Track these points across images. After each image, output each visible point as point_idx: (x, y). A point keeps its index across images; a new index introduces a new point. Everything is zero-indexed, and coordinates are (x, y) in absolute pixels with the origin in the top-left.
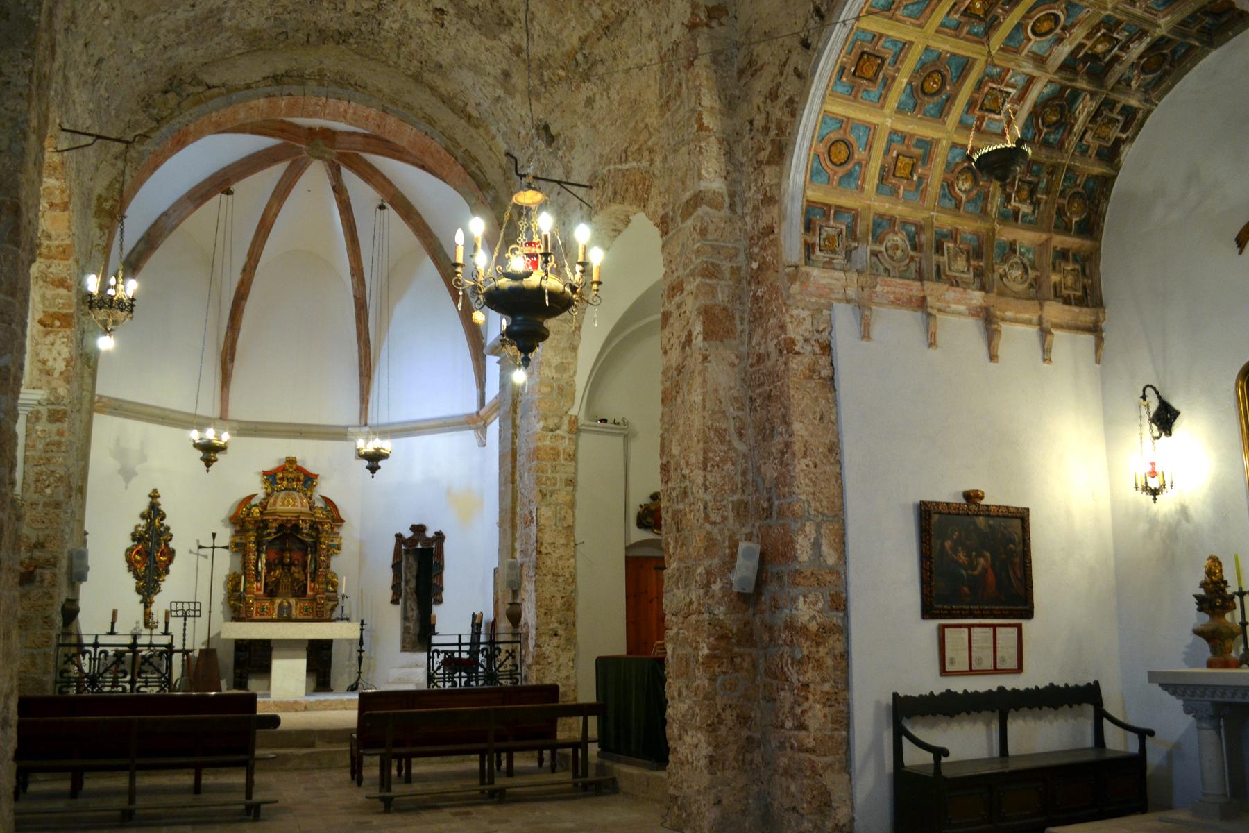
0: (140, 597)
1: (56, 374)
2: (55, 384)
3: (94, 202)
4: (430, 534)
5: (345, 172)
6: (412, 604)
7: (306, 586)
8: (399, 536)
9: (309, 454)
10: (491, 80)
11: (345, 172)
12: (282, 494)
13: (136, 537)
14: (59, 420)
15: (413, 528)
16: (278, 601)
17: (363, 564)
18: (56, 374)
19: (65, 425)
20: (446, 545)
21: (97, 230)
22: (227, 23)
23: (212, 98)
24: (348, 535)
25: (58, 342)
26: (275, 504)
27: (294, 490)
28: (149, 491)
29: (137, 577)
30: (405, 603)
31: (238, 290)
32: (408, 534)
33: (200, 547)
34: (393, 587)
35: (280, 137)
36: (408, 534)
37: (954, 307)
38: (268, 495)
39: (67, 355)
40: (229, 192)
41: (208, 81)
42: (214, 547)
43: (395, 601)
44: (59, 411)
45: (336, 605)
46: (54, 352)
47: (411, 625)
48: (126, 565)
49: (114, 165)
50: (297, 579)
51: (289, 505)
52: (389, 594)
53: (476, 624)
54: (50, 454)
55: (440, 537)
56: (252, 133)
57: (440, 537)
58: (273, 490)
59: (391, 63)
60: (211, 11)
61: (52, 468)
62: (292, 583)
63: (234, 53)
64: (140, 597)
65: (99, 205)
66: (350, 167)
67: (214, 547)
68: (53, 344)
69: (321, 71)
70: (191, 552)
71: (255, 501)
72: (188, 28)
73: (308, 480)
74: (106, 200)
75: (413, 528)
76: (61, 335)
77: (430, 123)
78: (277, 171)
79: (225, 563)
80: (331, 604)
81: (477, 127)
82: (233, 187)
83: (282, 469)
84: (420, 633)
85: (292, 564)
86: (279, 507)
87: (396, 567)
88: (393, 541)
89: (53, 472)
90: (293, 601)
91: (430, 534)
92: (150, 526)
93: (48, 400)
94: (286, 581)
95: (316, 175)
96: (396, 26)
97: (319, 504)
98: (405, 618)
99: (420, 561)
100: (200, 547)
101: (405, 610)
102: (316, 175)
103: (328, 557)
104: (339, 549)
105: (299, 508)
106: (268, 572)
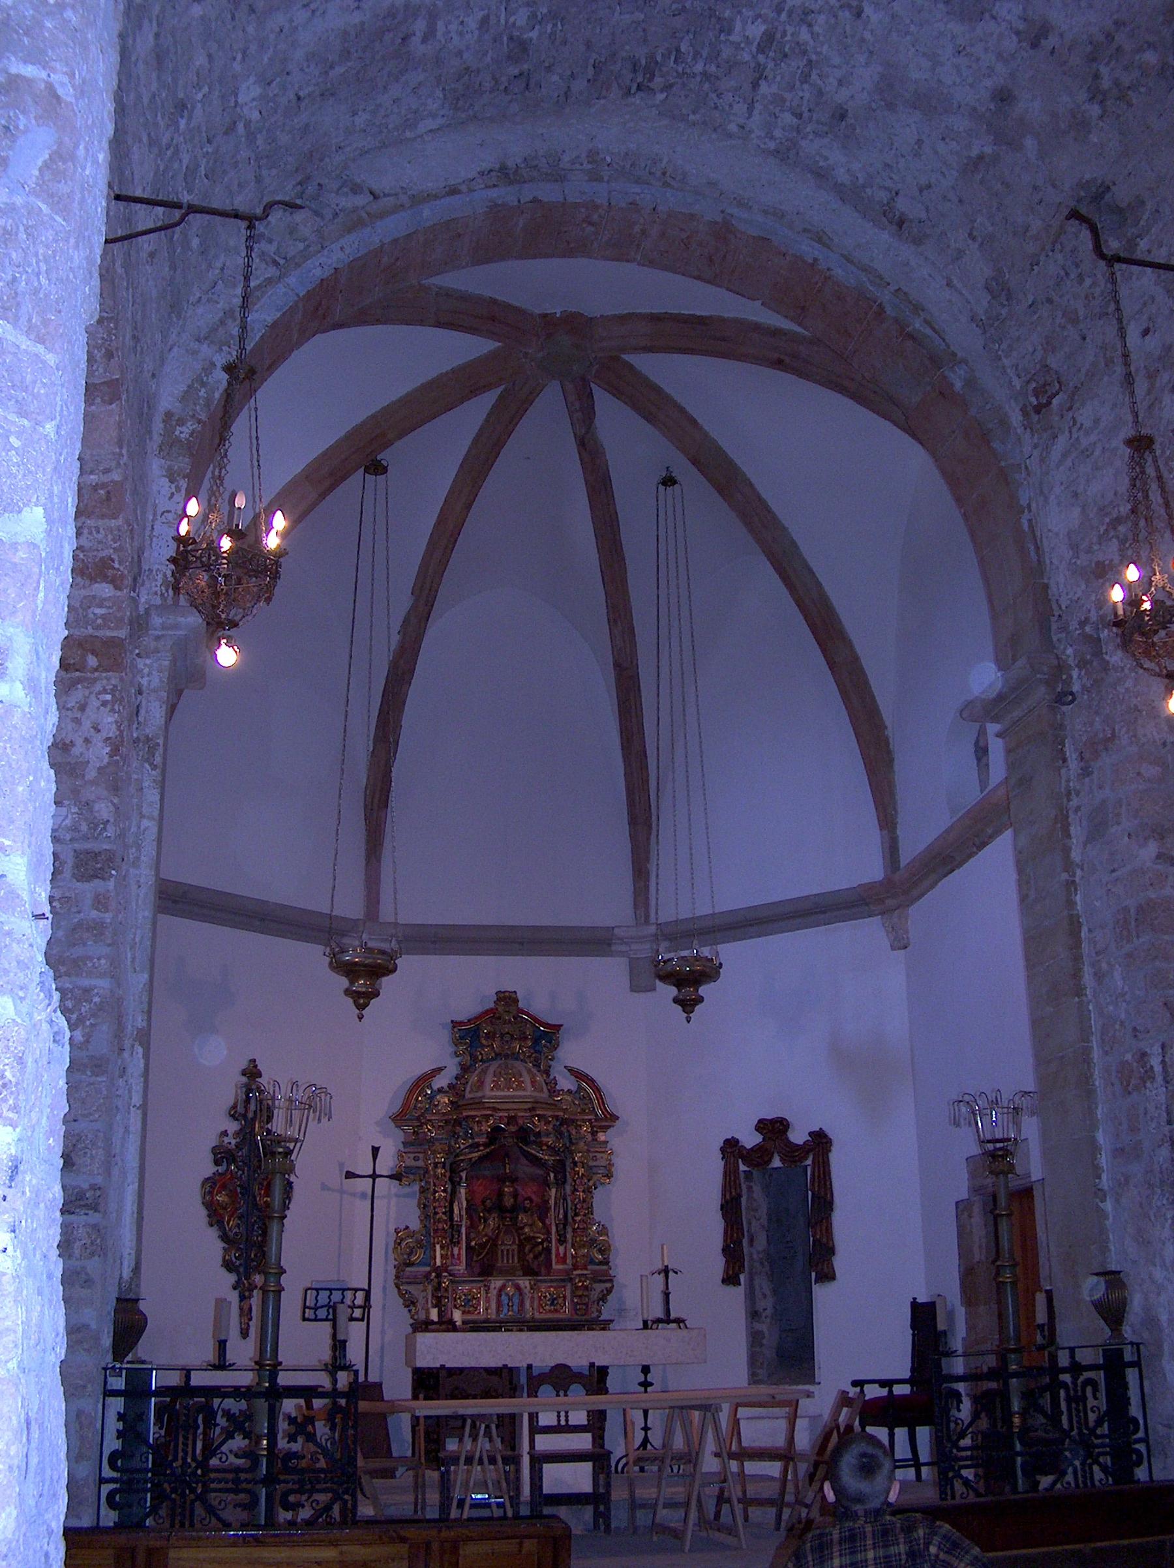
0: (232, 1278)
1: (91, 774)
2: (89, 793)
3: (158, 426)
4: (798, 1136)
5: (604, 402)
6: (763, 1284)
7: (548, 1250)
8: (731, 1148)
9: (541, 985)
10: (961, 123)
11: (604, 402)
12: (494, 1066)
13: (221, 1155)
14: (98, 875)
15: (763, 1126)
16: (496, 1283)
17: (657, 1205)
18: (91, 774)
19: (111, 884)
20: (836, 1158)
21: (165, 481)
22: (417, 47)
23: (382, 215)
24: (626, 1147)
25: (94, 703)
26: (481, 1083)
27: (515, 1056)
28: (244, 1064)
29: (224, 1237)
30: (751, 1280)
31: (394, 666)
32: (751, 1140)
33: (350, 1175)
34: (726, 1250)
35: (492, 335)
36: (751, 1140)
37: (282, 1477)
38: (465, 1069)
39: (113, 732)
40: (377, 468)
41: (375, 187)
42: (374, 1176)
43: (730, 1279)
44: (97, 854)
45: (609, 1291)
46: (87, 724)
47: (763, 1327)
48: (203, 1212)
49: (195, 353)
50: (530, 1239)
51: (505, 1091)
52: (718, 1264)
53: (923, 1316)
54: (78, 951)
55: (820, 1141)
56: (438, 325)
57: (820, 1141)
58: (474, 1058)
59: (733, 127)
60: (391, 13)
61: (86, 982)
62: (521, 1246)
63: (422, 128)
64: (232, 1278)
65: (168, 432)
66: (616, 392)
67: (374, 1176)
68: (83, 708)
69: (592, 155)
70: (324, 1187)
71: (441, 1082)
72: (346, 54)
73: (543, 1038)
74: (181, 422)
75: (763, 1126)
76: (98, 687)
77: (820, 241)
78: (474, 414)
79: (398, 1208)
80: (599, 1287)
81: (918, 241)
82: (384, 456)
83: (490, 1015)
84: (788, 1352)
85: (515, 1209)
86: (490, 1093)
87: (731, 1208)
88: (715, 1166)
89: (87, 990)
90: (525, 1283)
91: (798, 1136)
92: (246, 1135)
93: (75, 828)
94: (508, 1244)
95: (547, 422)
96: (757, 30)
97: (566, 1083)
98: (754, 1314)
99: (780, 1198)
100: (350, 1175)
101: (751, 1296)
102: (547, 422)
103: (588, 1191)
104: (609, 1176)
105: (529, 1091)
106: (472, 1227)
